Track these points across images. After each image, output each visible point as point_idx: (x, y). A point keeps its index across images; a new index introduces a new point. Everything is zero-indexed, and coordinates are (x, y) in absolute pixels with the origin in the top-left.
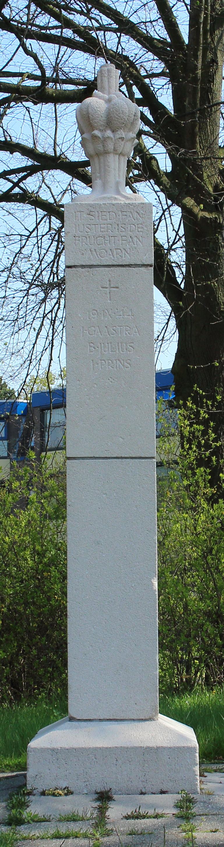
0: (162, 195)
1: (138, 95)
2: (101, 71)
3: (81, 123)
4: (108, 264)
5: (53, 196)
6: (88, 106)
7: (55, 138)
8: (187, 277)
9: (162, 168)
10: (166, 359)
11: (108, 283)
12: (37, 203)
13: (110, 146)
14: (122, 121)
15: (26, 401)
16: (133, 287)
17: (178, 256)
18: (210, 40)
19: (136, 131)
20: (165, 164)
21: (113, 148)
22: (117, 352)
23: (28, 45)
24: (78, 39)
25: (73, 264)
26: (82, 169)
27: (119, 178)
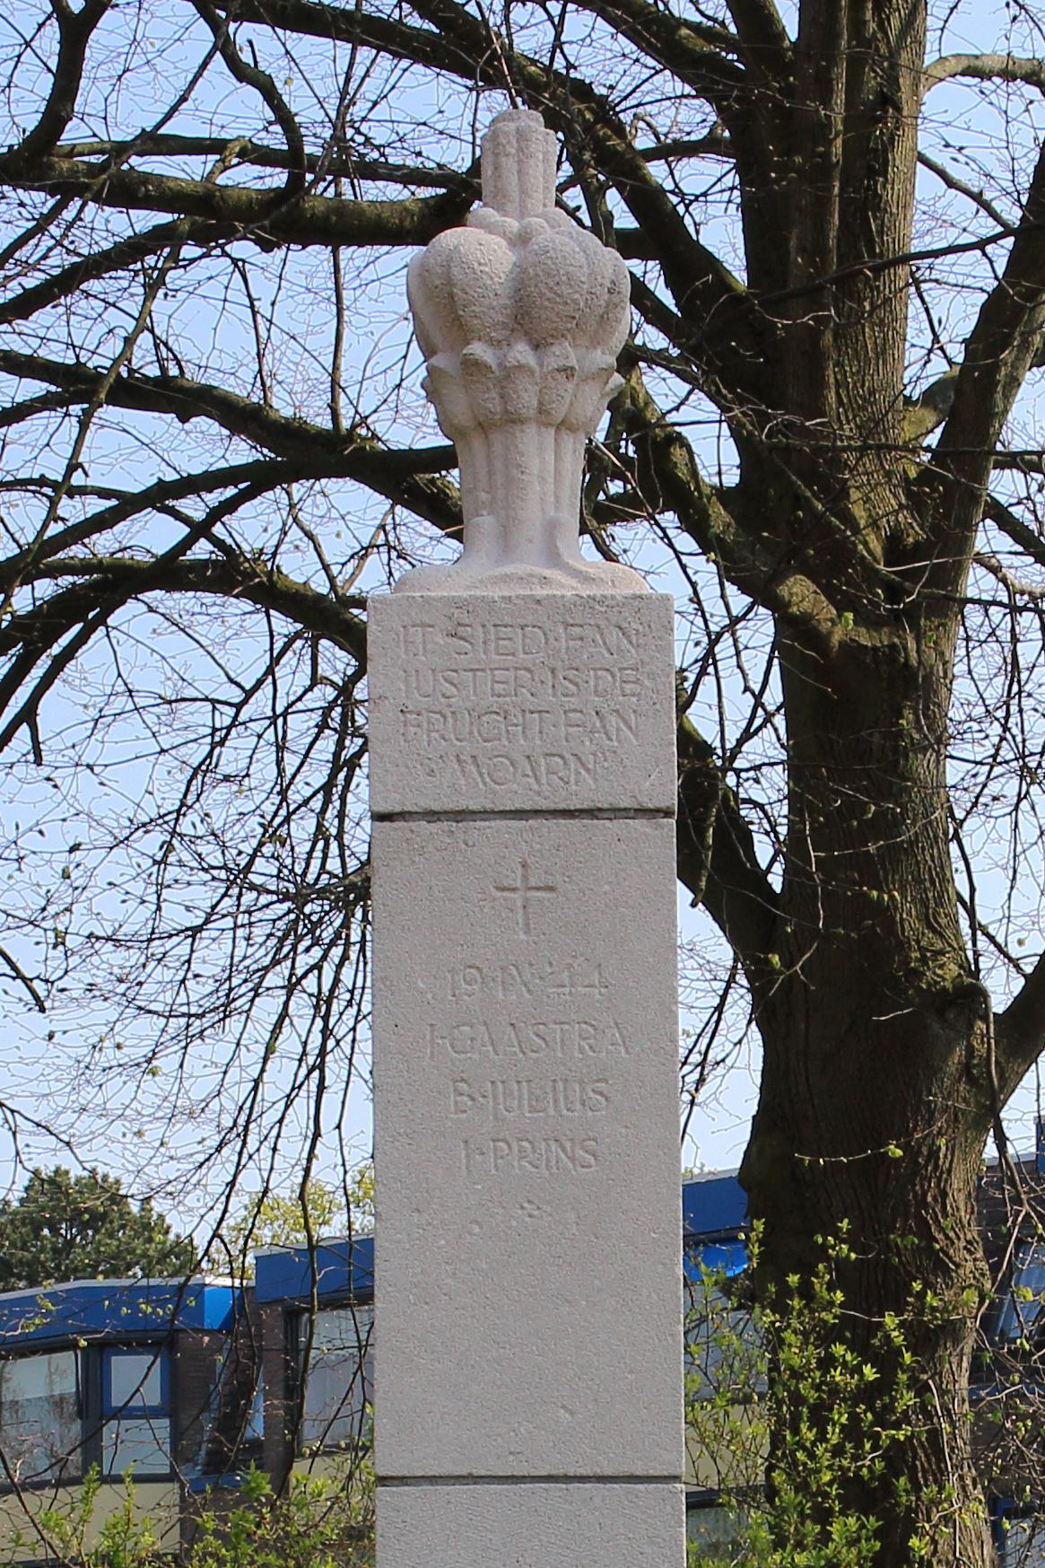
0: (705, 570)
1: (625, 219)
2: (494, 136)
3: (424, 316)
4: (518, 806)
5: (326, 568)
6: (450, 259)
7: (336, 366)
8: (792, 850)
9: (708, 475)
10: (718, 1137)
11: (520, 871)
12: (272, 593)
13: (527, 398)
14: (570, 310)
15: (228, 1282)
16: (606, 887)
17: (765, 788)
18: (872, 26)
19: (618, 342)
20: (715, 455)
21: (535, 403)
22: (552, 1113)
23: (240, 40)
24: (415, 21)
25: (398, 809)
26: (428, 476)
27: (557, 509)
